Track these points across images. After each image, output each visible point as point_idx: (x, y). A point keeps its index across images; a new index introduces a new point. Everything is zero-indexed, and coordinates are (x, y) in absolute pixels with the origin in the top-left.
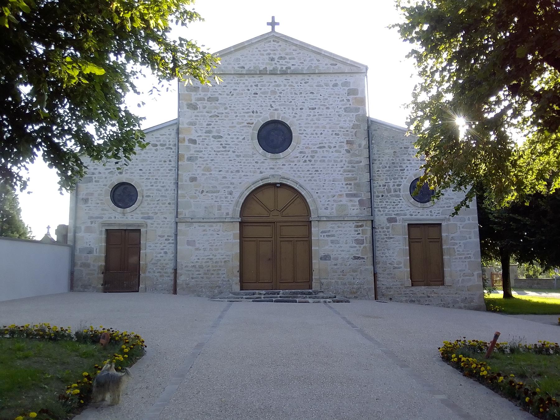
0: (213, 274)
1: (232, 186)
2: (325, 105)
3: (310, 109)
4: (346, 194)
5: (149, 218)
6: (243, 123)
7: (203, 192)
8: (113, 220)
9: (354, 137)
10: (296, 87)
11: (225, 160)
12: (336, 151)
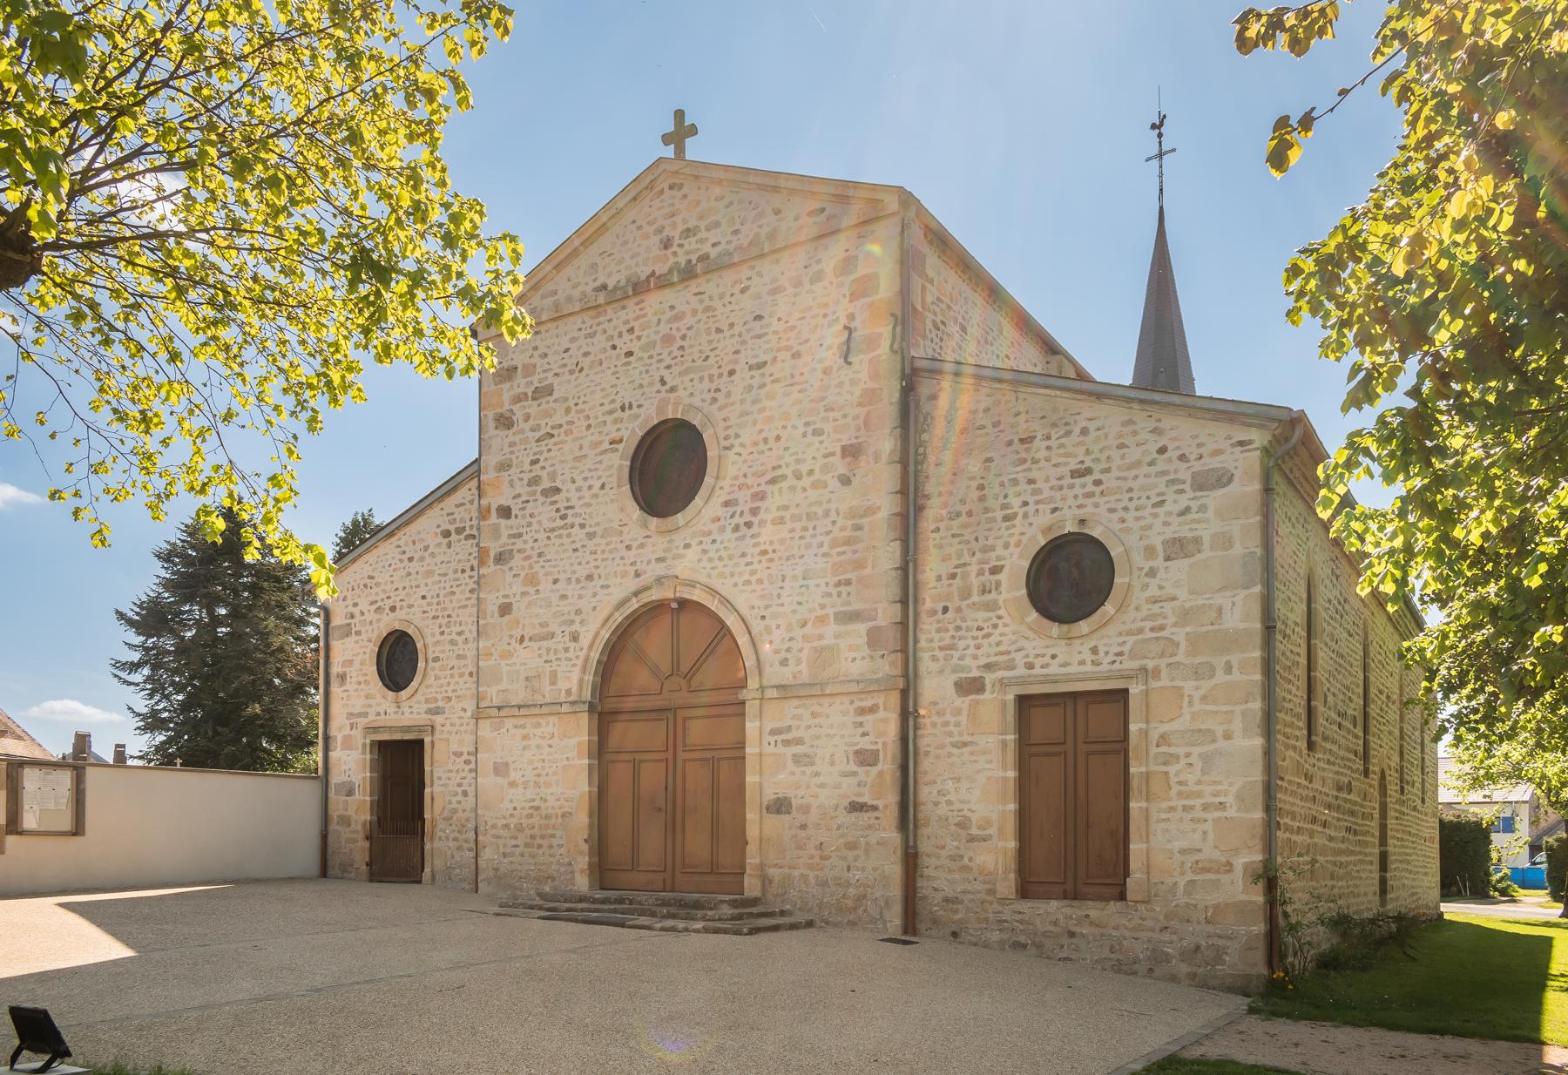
0: (540, 846)
1: (578, 619)
3: (751, 368)
4: (836, 614)
6: (601, 443)
7: (522, 639)
8: (382, 721)
12: (814, 486)
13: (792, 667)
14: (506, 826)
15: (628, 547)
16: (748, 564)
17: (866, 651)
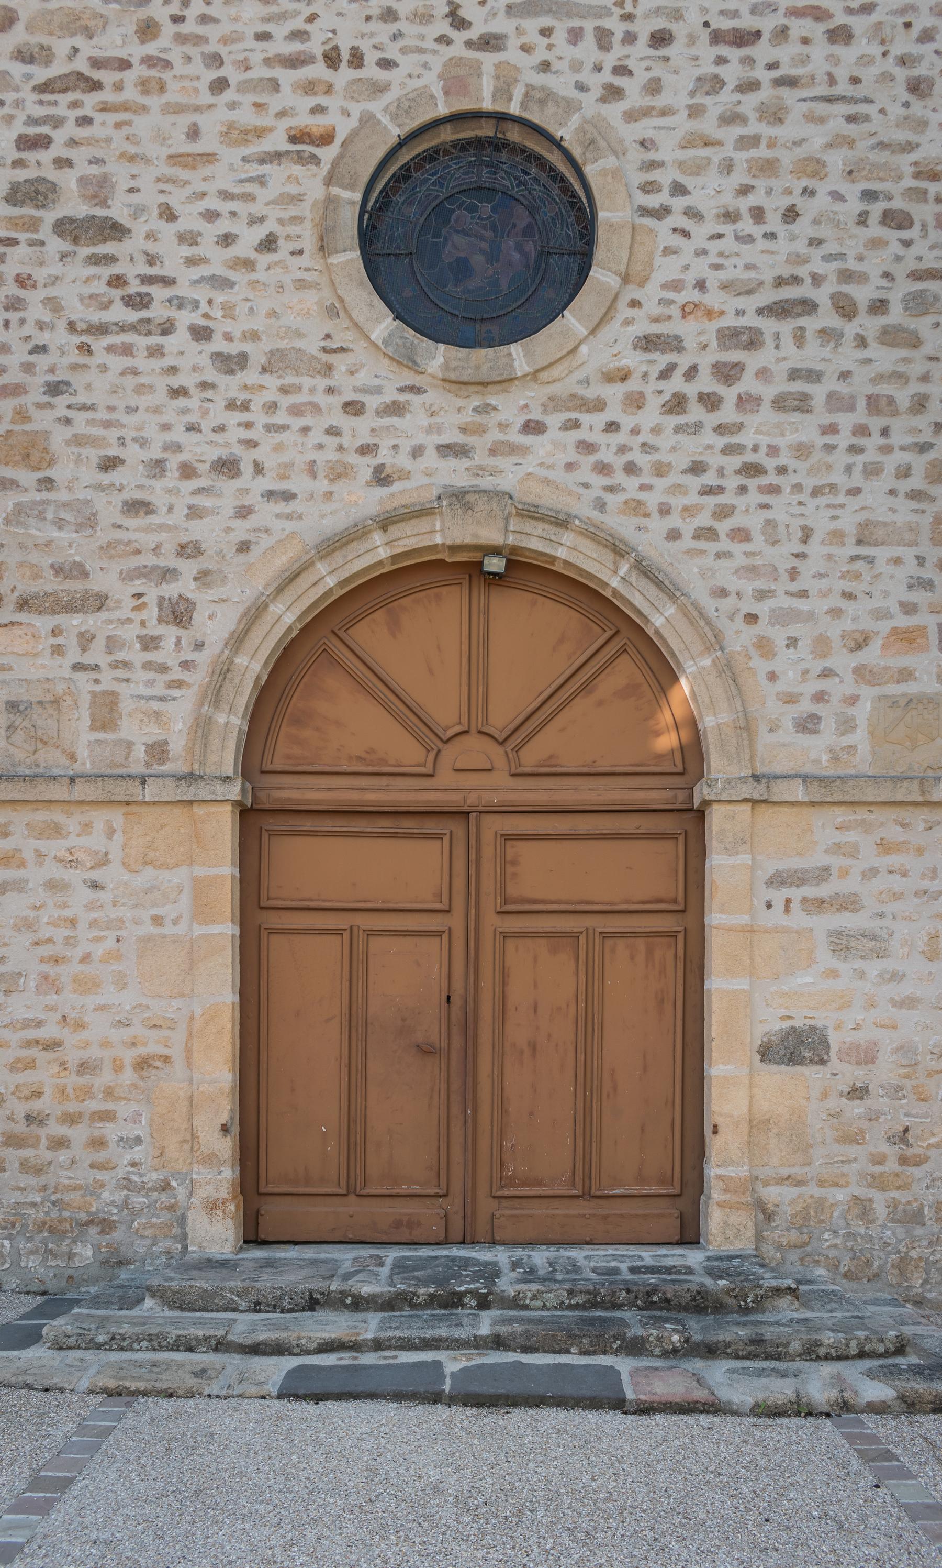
1: (188, 568)
6: (260, 133)
12: (890, 337)
13: (828, 736)
15: (353, 408)
16: (708, 491)
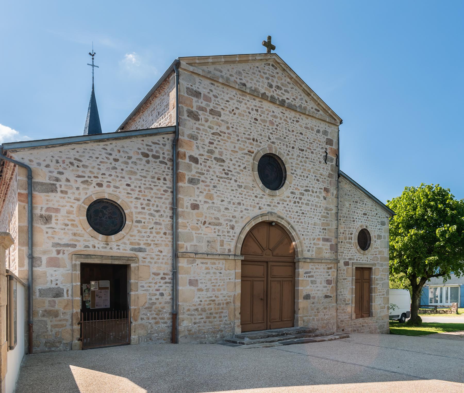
0: (215, 317)
1: (234, 220)
2: (311, 149)
4: (323, 238)
5: (140, 250)
6: (244, 149)
7: (205, 223)
8: (91, 251)
9: (329, 185)
10: (290, 124)
11: (227, 189)
14: (197, 310)
17: (330, 251)
